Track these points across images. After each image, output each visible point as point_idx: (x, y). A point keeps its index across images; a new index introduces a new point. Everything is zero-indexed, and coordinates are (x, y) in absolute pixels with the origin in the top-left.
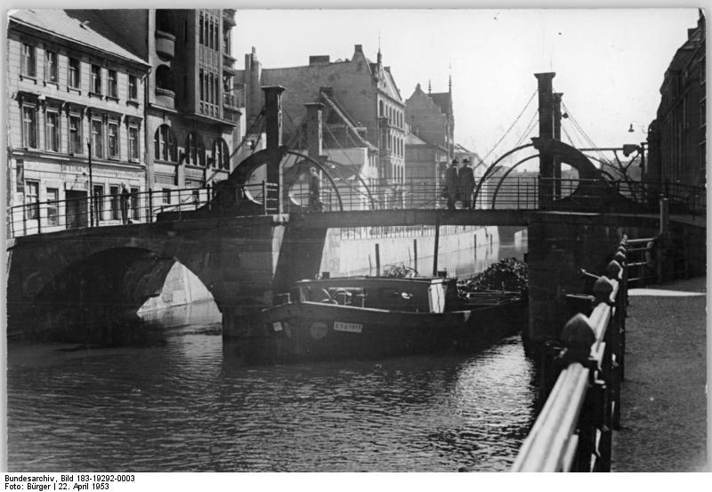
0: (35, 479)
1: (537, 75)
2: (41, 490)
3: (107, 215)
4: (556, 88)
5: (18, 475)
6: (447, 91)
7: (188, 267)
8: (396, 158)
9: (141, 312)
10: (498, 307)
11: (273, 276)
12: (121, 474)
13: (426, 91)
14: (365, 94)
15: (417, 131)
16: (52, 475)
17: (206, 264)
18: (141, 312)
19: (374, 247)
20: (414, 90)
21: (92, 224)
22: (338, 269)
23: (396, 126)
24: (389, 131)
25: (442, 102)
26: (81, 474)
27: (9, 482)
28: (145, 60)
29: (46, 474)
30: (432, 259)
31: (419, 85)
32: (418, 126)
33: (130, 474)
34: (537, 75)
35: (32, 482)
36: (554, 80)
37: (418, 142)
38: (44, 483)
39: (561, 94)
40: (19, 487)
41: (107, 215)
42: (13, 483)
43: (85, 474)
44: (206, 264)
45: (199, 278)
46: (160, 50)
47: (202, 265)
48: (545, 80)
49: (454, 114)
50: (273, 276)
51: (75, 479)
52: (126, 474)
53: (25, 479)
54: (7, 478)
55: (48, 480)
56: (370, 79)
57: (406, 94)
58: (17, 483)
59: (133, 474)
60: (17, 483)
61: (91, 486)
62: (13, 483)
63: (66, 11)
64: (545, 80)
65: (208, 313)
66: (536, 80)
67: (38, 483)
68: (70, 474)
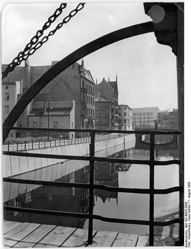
0: (187, 237)
3: (85, 128)
5: (185, 243)
12: (185, 207)
13: (107, 80)
14: (76, 78)
15: (103, 96)
16: (185, 231)
20: (102, 80)
21: (82, 133)
22: (119, 171)
23: (91, 92)
25: (114, 85)
29: (185, 233)
30: (69, 239)
31: (104, 78)
32: (103, 94)
33: (185, 203)
39: (104, 203)
41: (85, 128)
42: (188, 245)
43: (185, 219)
49: (118, 90)
51: (186, 223)
52: (185, 205)
53: (186, 240)
54: (186, 247)
55: (187, 232)
56: (78, 72)
58: (188, 243)
60: (188, 243)
62: (188, 245)
67: (188, 236)
68: (185, 225)
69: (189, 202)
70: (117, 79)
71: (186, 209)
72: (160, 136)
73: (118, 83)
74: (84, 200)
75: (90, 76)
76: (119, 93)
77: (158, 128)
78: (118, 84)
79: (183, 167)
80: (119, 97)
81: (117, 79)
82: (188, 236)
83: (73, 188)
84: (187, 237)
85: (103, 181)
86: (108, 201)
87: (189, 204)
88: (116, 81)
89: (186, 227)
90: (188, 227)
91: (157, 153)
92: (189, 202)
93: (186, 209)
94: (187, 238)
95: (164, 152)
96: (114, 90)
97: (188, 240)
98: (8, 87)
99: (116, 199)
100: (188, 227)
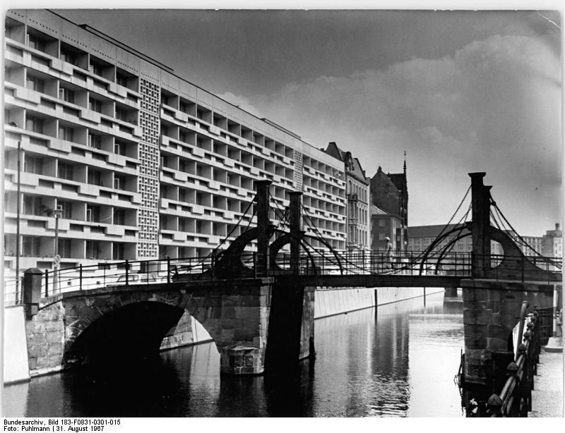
0: (27, 423)
1: (470, 175)
2: (77, 431)
4: (486, 182)
6: (403, 172)
7: (196, 318)
8: (361, 225)
9: (492, 241)
16: (41, 419)
17: (209, 316)
18: (492, 241)
19: (7, 388)
20: (376, 172)
24: (356, 204)
26: (64, 419)
27: (7, 425)
28: (20, 42)
29: (37, 419)
31: (380, 168)
34: (470, 175)
35: (25, 425)
36: (484, 178)
37: (380, 212)
39: (484, 174)
40: (15, 429)
42: (10, 426)
43: (68, 419)
44: (209, 316)
47: (206, 318)
53: (20, 423)
54: (5, 422)
55: (38, 423)
57: (371, 174)
58: (14, 426)
60: (14, 426)
61: (89, 429)
62: (10, 426)
66: (470, 178)
68: (56, 419)
69: (56, 428)
70: (405, 168)
71: (92, 421)
73: (407, 177)
76: (409, 197)
77: (237, 317)
78: (408, 180)
80: (409, 204)
81: (405, 168)
83: (245, 250)
84: (27, 423)
85: (524, 251)
87: (51, 429)
88: (403, 172)
89: (50, 422)
93: (108, 421)
94: (25, 425)
96: (400, 191)
97: (19, 427)
98: (400, 181)
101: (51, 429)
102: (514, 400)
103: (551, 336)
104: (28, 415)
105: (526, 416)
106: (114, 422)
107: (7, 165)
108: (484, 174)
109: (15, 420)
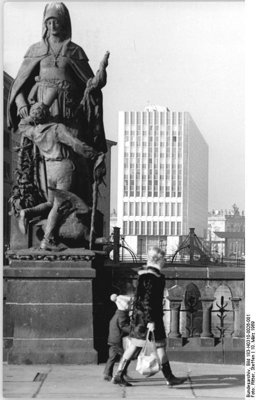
0: (249, 380)
10: (11, 190)
11: (145, 281)
12: (246, 331)
19: (220, 298)
26: (246, 355)
27: (250, 395)
38: (251, 376)
39: (194, 229)
42: (251, 393)
43: (246, 352)
45: (171, 371)
46: (27, 247)
48: (108, 56)
50: (145, 281)
51: (248, 358)
53: (249, 386)
54: (248, 396)
55: (249, 373)
58: (251, 390)
59: (246, 315)
60: (251, 390)
62: (251, 393)
63: (5, 73)
64: (108, 56)
65: (165, 310)
66: (189, 230)
68: (246, 361)
69: (253, 351)
71: (247, 349)
72: (181, 281)
74: (66, 117)
75: (47, 34)
79: (66, 15)
82: (251, 379)
86: (224, 298)
87: (253, 354)
89: (248, 365)
90: (251, 364)
91: (177, 266)
92: (253, 351)
93: (247, 349)
95: (230, 349)
97: (251, 386)
99: (97, 209)
100: (251, 364)
101: (253, 354)
102: (94, 114)
103: (94, 278)
104: (244, 384)
105: (4, 360)
106: (248, 339)
107: (145, 196)
108: (194, 229)
109: (246, 390)
